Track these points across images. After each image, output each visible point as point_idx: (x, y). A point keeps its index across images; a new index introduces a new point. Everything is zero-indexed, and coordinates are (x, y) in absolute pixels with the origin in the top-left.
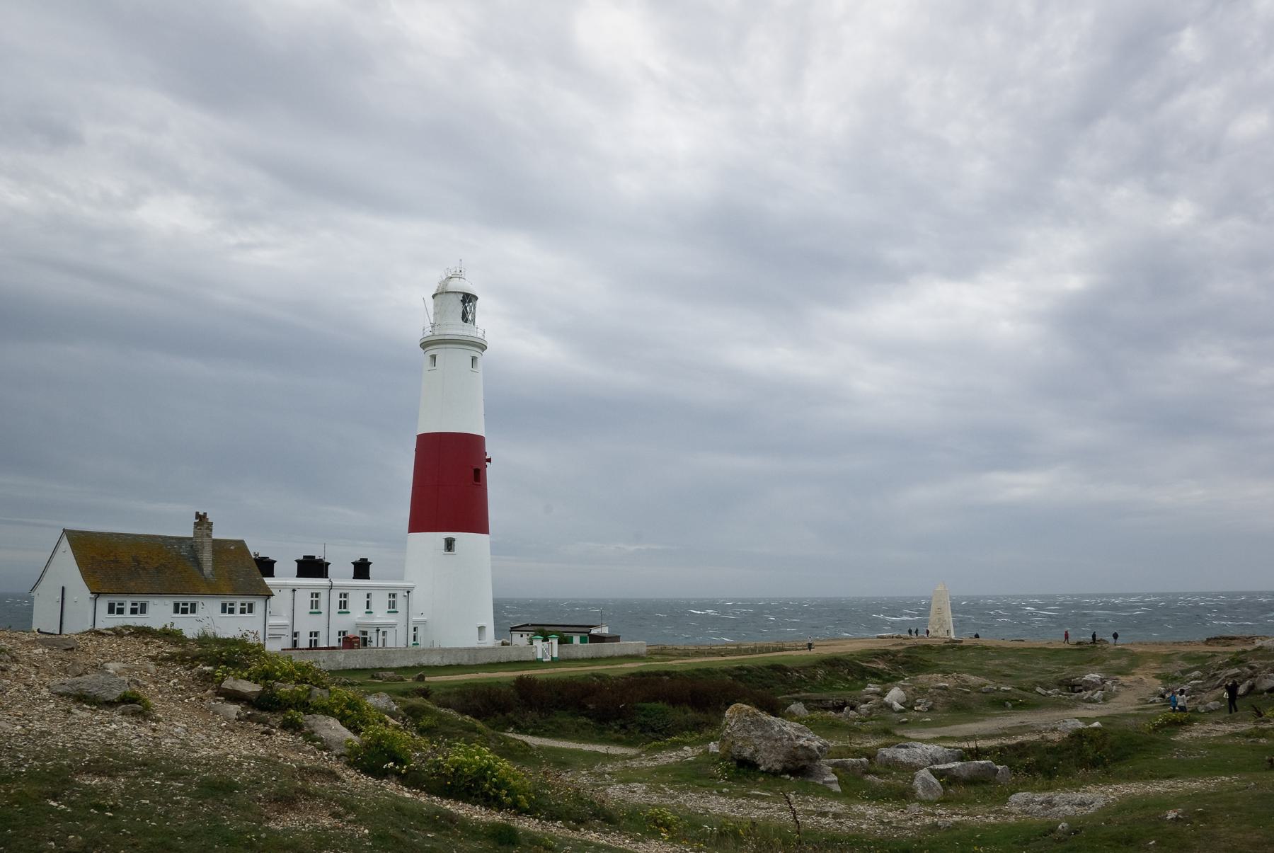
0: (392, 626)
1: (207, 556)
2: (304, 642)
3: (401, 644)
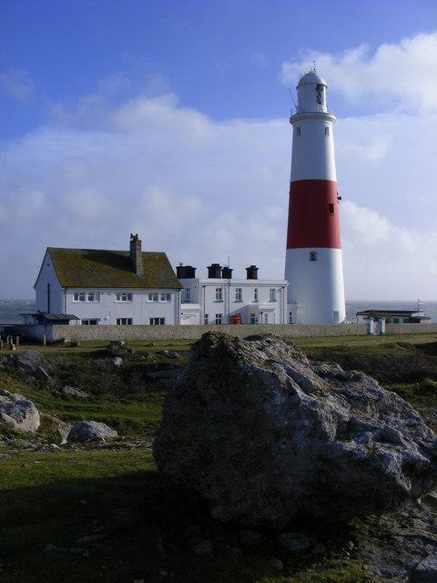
0: (271, 310)
1: (139, 261)
2: (212, 318)
3: (277, 322)
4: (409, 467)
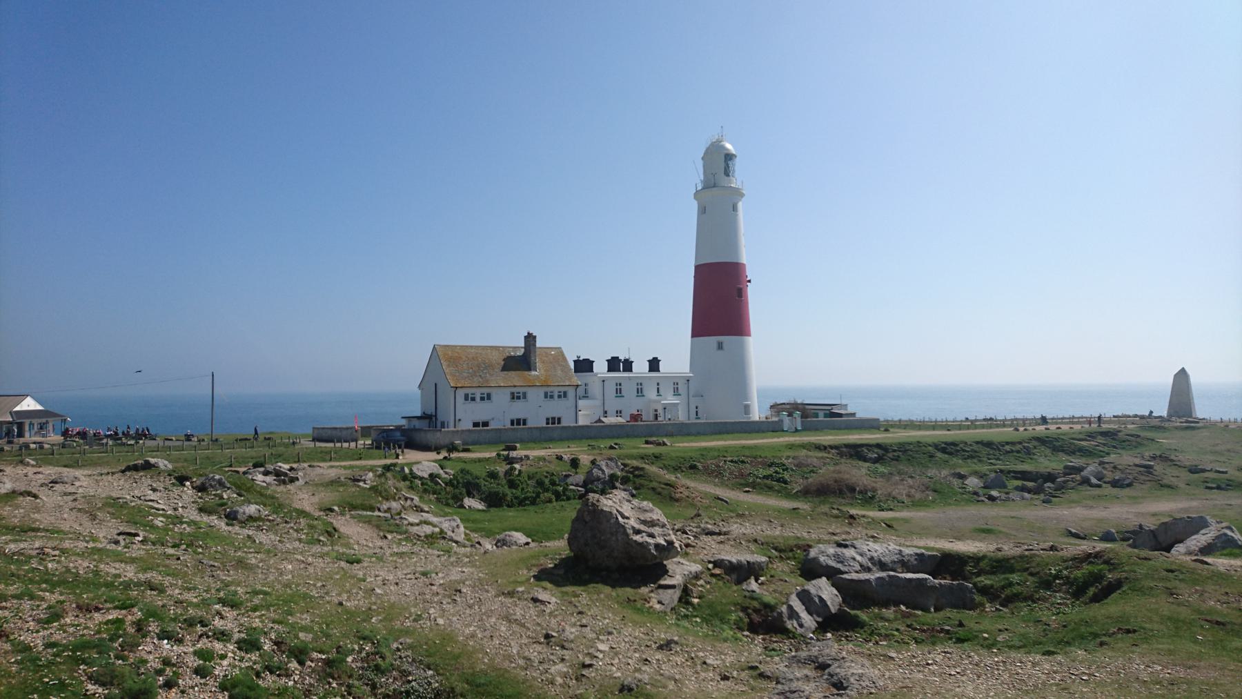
4: (657, 546)
